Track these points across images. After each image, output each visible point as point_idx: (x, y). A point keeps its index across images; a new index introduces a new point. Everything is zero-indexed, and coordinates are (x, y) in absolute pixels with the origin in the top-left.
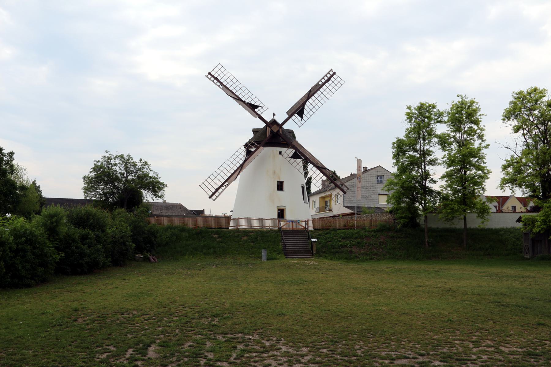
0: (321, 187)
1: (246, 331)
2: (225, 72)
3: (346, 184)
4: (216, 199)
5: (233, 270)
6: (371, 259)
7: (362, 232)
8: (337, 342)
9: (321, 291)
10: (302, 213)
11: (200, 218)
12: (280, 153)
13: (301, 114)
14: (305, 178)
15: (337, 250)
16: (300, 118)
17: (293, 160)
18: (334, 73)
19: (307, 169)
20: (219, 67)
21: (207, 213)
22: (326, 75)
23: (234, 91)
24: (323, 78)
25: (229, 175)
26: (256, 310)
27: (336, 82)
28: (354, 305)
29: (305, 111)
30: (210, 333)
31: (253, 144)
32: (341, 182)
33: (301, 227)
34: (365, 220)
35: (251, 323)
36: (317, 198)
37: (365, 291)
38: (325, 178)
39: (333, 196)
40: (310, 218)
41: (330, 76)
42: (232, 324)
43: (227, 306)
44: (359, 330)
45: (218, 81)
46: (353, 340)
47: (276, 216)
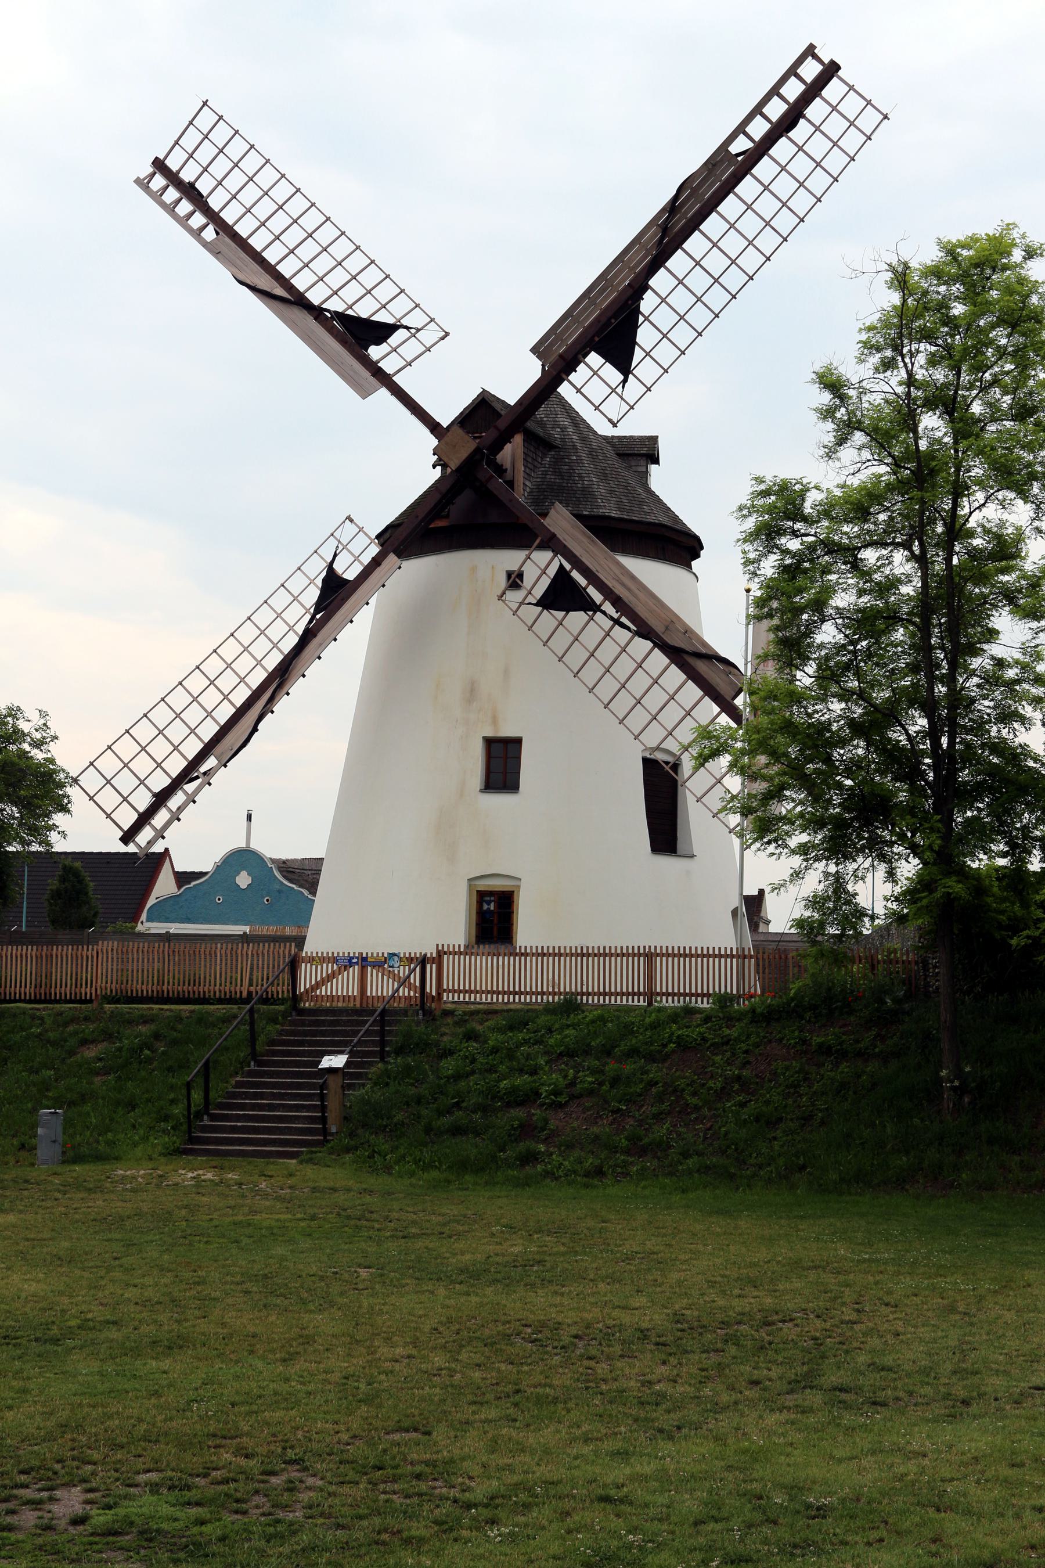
16: (612, 374)
45: (199, 201)
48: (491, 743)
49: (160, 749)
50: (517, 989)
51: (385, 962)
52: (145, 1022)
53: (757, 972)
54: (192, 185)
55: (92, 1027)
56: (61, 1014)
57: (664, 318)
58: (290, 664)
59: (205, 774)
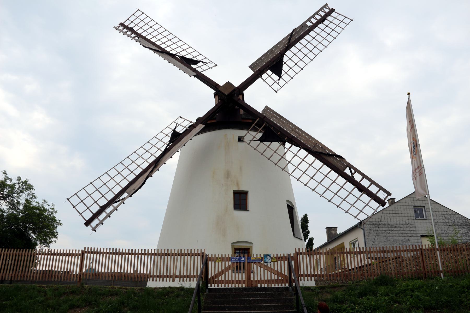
16: (276, 77)
18: (332, 11)
33: (274, 277)
48: (237, 193)
49: (104, 190)
51: (262, 260)
52: (111, 295)
55: (77, 297)
56: (57, 289)
57: (290, 63)
58: (159, 160)
59: (122, 199)
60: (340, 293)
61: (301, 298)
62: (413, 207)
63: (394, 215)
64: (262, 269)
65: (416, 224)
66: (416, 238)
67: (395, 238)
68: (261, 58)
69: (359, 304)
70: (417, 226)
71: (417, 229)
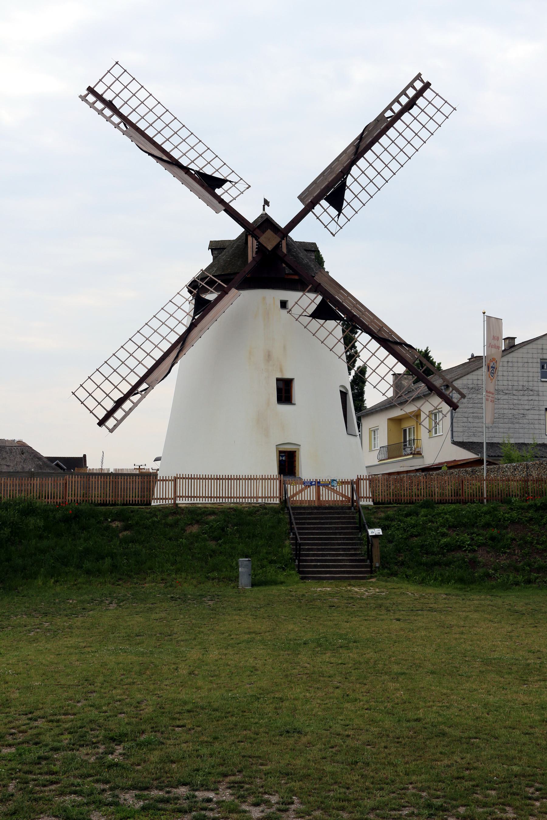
0: (390, 394)
1: (199, 779)
2: (134, 87)
3: (458, 384)
4: (115, 426)
5: (163, 615)
6: (529, 582)
7: (503, 511)
8: (441, 808)
9: (396, 668)
10: (343, 459)
11: (75, 479)
12: (284, 304)
13: (337, 201)
14: (350, 369)
15: (437, 558)
16: (333, 212)
17: (316, 323)
18: (427, 85)
19: (354, 347)
20: (117, 71)
21: (92, 465)
22: (404, 93)
23: (159, 140)
24: (397, 100)
25: (150, 363)
26: (224, 721)
27: (431, 110)
28: (486, 705)
29: (347, 192)
30: (101, 786)
31: (211, 283)
32: (444, 379)
34: (510, 477)
35: (211, 755)
36: (381, 423)
37: (515, 668)
38: (401, 369)
39: (423, 416)
40: (364, 473)
41: (417, 92)
42: (162, 761)
43: (148, 710)
44: (503, 775)
46: (485, 805)
47: (273, 470)
50: (230, 496)
51: (330, 484)
53: (370, 486)
54: (111, 102)
60: (392, 513)
61: (363, 514)
62: (539, 361)
63: (505, 374)
64: (330, 492)
65: (541, 389)
66: (537, 412)
67: (501, 411)
68: (314, 182)
69: (404, 522)
70: (541, 393)
71: (541, 398)
